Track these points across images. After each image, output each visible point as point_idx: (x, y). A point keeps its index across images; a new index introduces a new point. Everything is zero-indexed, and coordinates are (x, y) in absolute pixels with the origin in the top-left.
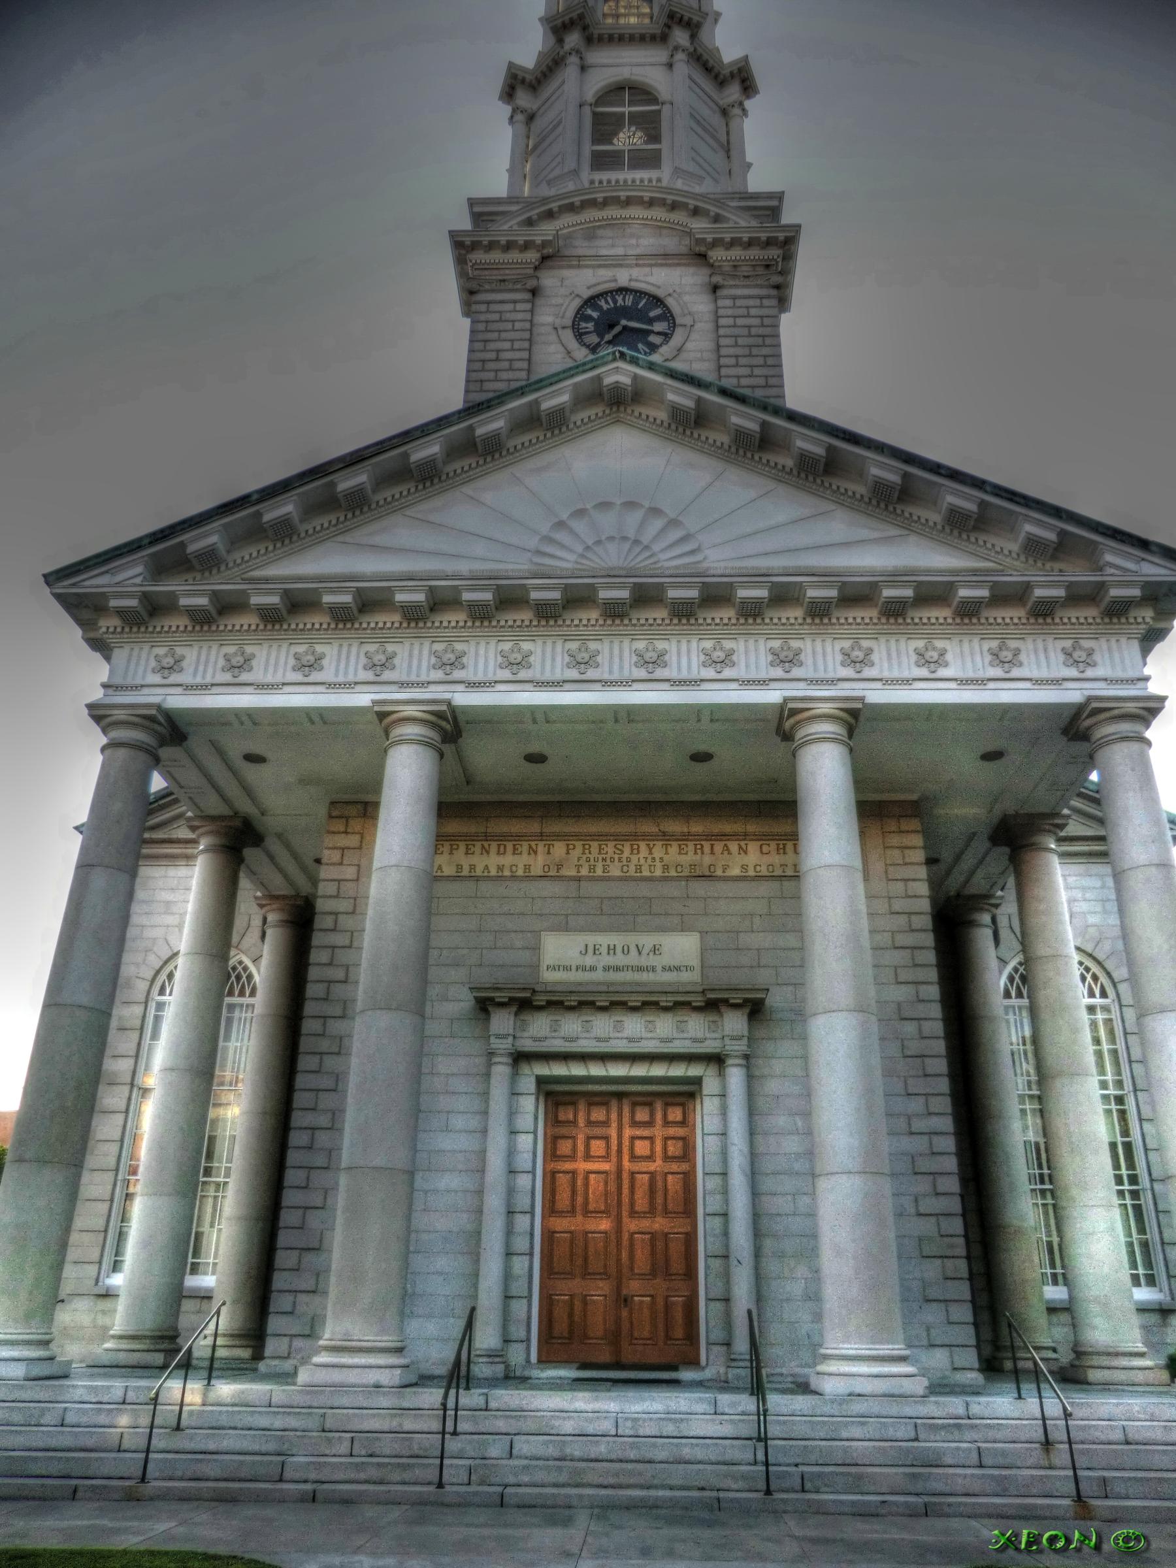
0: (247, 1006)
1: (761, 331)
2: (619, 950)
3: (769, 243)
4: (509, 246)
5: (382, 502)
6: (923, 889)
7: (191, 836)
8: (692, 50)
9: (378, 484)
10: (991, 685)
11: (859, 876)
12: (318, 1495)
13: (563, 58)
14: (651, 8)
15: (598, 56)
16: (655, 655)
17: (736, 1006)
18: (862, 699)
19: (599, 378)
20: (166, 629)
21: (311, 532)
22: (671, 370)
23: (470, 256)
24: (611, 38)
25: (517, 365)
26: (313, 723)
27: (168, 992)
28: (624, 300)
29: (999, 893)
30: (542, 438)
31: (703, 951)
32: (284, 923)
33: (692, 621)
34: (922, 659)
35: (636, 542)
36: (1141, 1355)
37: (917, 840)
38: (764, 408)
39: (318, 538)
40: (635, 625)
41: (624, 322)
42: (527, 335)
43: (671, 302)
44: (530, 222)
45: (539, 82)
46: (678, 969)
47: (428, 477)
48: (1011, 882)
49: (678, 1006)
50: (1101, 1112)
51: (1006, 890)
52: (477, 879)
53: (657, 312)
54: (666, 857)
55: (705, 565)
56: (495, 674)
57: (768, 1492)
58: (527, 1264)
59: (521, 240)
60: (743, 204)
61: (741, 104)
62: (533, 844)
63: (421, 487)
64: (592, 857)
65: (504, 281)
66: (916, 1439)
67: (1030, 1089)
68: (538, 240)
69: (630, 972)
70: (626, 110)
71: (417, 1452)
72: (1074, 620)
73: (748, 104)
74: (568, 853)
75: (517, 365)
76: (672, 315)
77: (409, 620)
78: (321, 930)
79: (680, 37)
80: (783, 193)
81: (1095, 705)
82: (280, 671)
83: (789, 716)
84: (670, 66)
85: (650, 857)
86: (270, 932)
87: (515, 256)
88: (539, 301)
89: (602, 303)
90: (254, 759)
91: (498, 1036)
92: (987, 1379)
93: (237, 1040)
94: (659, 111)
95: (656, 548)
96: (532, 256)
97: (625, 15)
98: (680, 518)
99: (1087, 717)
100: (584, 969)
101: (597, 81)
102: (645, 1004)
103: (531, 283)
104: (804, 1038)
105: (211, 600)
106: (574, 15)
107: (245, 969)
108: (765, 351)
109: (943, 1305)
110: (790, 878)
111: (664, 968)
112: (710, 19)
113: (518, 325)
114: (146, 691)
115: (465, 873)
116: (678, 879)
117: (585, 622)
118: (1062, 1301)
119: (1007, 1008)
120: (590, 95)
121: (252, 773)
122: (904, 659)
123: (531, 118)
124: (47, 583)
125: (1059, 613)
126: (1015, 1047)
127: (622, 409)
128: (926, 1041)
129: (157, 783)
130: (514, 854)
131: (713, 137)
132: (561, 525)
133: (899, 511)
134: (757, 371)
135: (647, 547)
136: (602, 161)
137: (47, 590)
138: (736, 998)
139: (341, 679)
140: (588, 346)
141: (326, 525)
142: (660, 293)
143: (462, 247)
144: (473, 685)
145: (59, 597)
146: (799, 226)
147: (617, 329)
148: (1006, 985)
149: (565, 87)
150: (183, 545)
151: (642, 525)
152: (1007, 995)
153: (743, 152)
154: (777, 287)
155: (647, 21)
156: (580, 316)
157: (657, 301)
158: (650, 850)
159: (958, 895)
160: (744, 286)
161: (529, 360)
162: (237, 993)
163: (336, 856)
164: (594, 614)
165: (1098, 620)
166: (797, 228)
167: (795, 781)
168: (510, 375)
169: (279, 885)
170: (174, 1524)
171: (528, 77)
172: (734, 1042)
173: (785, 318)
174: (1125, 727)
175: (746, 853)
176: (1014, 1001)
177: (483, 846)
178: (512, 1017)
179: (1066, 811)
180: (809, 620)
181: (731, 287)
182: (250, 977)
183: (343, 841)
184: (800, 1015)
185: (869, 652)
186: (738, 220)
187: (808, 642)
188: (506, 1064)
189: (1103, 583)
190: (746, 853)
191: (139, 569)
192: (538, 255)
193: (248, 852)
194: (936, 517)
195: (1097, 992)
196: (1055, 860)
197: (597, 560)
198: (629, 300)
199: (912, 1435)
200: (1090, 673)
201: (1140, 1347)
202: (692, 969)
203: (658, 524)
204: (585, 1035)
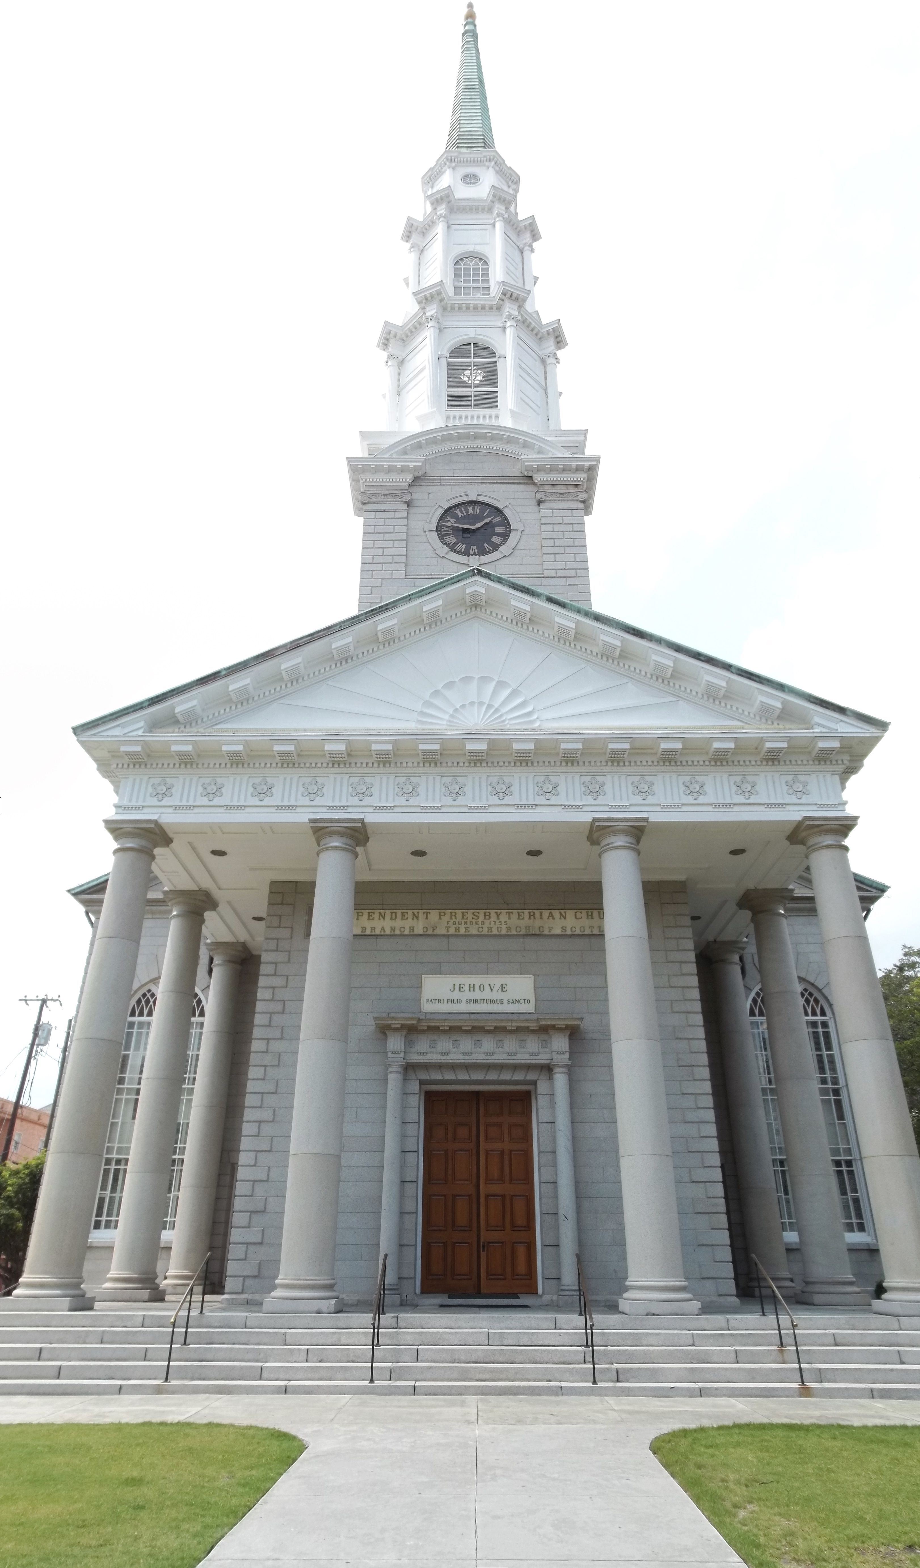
1: (572, 535)
2: (477, 988)
3: (578, 469)
10: (736, 808)
12: (288, 1389)
17: (560, 1030)
22: (513, 583)
26: (264, 832)
28: (473, 510)
29: (745, 939)
36: (851, 1283)
38: (579, 611)
43: (507, 512)
46: (519, 1002)
49: (519, 1030)
50: (819, 1104)
53: (498, 519)
54: (509, 921)
57: (782, 1345)
58: (414, 1220)
59: (399, 465)
61: (555, 354)
66: (693, 1345)
67: (770, 1084)
70: (472, 360)
71: (352, 1358)
74: (440, 918)
76: (508, 522)
79: (510, 308)
80: (587, 430)
81: (808, 823)
83: (597, 831)
85: (497, 921)
88: (412, 510)
89: (458, 512)
91: (394, 1052)
92: (741, 1301)
96: (408, 478)
100: (453, 1001)
102: (497, 1029)
103: (407, 498)
109: (824, 991)
115: (368, 932)
118: (796, 1243)
119: (752, 1023)
124: (75, 733)
127: (478, 609)
128: (694, 1055)
132: (436, 693)
137: (75, 738)
138: (561, 1024)
139: (286, 803)
140: (447, 545)
142: (500, 506)
145: (82, 743)
148: (751, 1007)
152: (752, 1013)
154: (583, 502)
158: (498, 916)
159: (715, 941)
162: (197, 1014)
166: (597, 459)
170: (200, 1409)
172: (559, 1056)
174: (829, 840)
175: (565, 918)
177: (380, 914)
184: (605, 1034)
185: (651, 785)
186: (555, 452)
187: (609, 777)
190: (565, 918)
191: (142, 724)
195: (818, 1012)
198: (477, 510)
199: (691, 1342)
200: (804, 800)
201: (850, 1277)
202: (529, 1001)
204: (454, 1050)
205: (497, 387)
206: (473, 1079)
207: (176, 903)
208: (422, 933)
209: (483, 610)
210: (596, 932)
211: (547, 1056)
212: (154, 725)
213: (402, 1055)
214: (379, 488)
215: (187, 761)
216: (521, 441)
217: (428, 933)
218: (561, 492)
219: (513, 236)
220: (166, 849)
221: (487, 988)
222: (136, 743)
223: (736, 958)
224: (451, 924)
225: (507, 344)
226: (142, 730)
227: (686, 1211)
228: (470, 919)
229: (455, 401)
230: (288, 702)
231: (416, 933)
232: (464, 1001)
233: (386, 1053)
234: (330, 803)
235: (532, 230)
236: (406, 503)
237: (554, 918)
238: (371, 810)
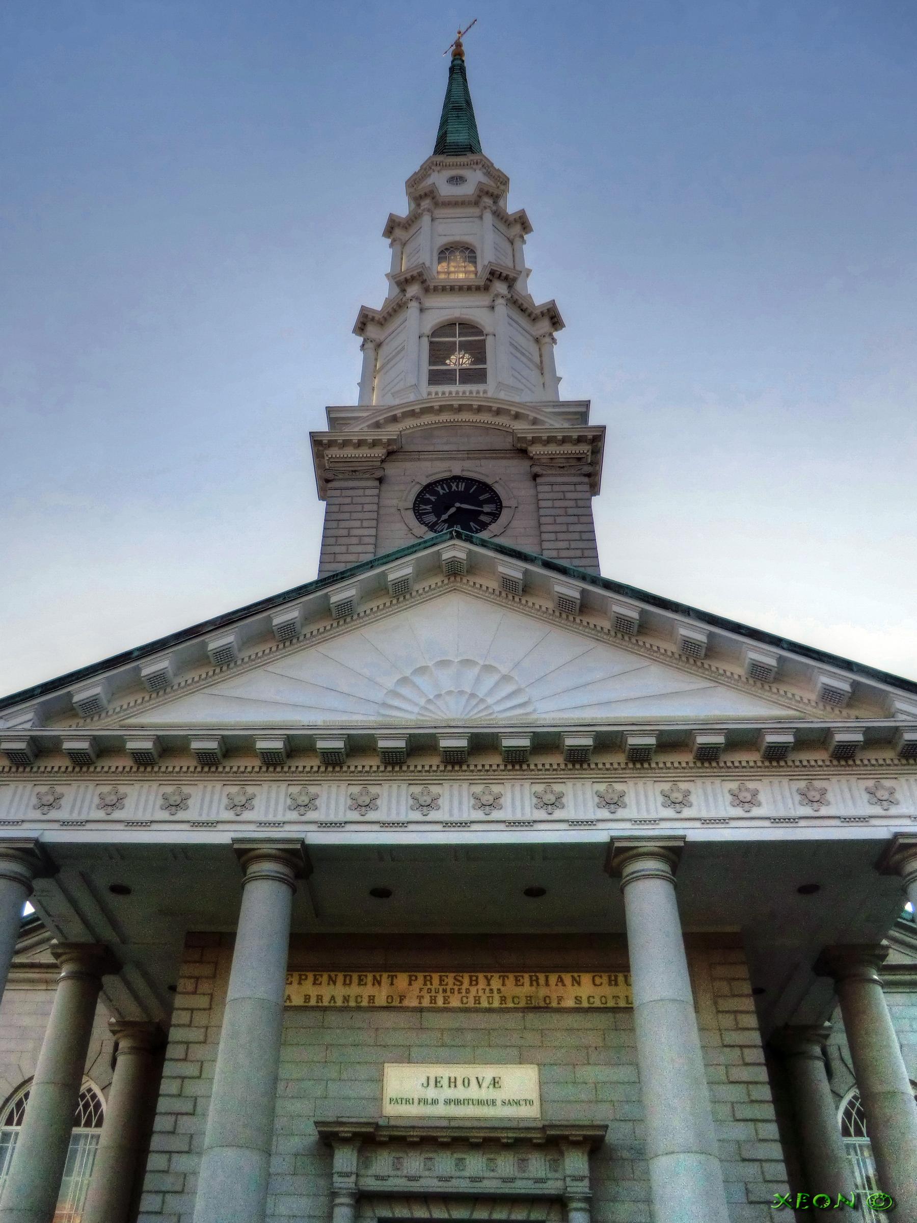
0: (93, 1136)
1: (576, 511)
2: (459, 1082)
3: (580, 440)
4: (360, 444)
5: (246, 659)
6: (752, 1021)
7: (52, 960)
8: (509, 296)
9: (244, 644)
10: (802, 823)
11: (691, 1009)
13: (405, 303)
14: (476, 267)
15: (432, 301)
16: (491, 798)
18: (683, 838)
19: (438, 553)
20: (49, 769)
21: (183, 684)
22: (501, 546)
23: (327, 452)
24: (444, 289)
25: (366, 540)
27: (16, 1119)
28: (457, 486)
29: (827, 1024)
30: (388, 604)
31: (541, 1084)
32: (134, 1050)
33: (525, 767)
34: (738, 800)
35: (473, 695)
37: (742, 971)
38: (584, 578)
39: (191, 688)
40: (472, 771)
41: (458, 505)
42: (375, 515)
43: (498, 488)
44: (377, 425)
45: (385, 319)
46: (518, 1103)
47: (288, 636)
48: (838, 1013)
51: (833, 1021)
52: (325, 1009)
53: (487, 496)
54: (503, 989)
55: (534, 716)
56: (345, 815)
59: (370, 439)
60: (557, 410)
61: (551, 334)
62: (378, 975)
63: (281, 646)
64: (433, 988)
65: (355, 471)
68: (385, 438)
69: (471, 1106)
70: (457, 339)
72: (873, 762)
73: (556, 334)
74: (410, 984)
75: (366, 540)
76: (499, 498)
77: (268, 765)
78: (172, 1060)
79: (500, 287)
82: (149, 810)
83: (616, 855)
84: (492, 308)
86: (121, 1060)
87: (364, 452)
88: (385, 487)
89: (439, 489)
90: (119, 890)
93: (79, 1175)
94: (484, 340)
95: (490, 701)
96: (380, 452)
97: (454, 272)
98: (512, 674)
99: (895, 854)
101: (433, 319)
103: (379, 474)
104: (646, 1177)
105: (91, 745)
106: (415, 273)
107: (94, 1097)
108: (579, 528)
110: (623, 1013)
111: (504, 1103)
112: (524, 274)
113: (367, 508)
114: (26, 826)
115: (313, 1002)
116: (516, 1010)
117: (427, 768)
119: (848, 1146)
120: (428, 328)
121: (116, 902)
122: (720, 799)
123: (379, 345)
125: (859, 755)
126: (861, 1191)
127: (458, 579)
129: (29, 909)
130: (359, 984)
131: (530, 360)
132: (404, 680)
133: (706, 666)
134: (574, 545)
135: (482, 700)
136: (436, 378)
140: (426, 525)
141: (196, 679)
142: (489, 481)
143: (318, 443)
144: (325, 825)
146: (604, 427)
147: (452, 510)
149: (406, 323)
150: (70, 695)
151: (478, 680)
152: (846, 1132)
153: (554, 370)
154: (589, 475)
155: (472, 276)
156: (420, 500)
157: (485, 487)
160: (560, 475)
161: (376, 536)
163: (189, 985)
164: (435, 761)
165: (896, 762)
167: (625, 923)
168: (360, 549)
169: (134, 1012)
171: (377, 317)
173: (595, 500)
175: (579, 984)
176: (854, 1140)
178: (355, 1154)
179: (885, 942)
180: (631, 765)
181: (548, 475)
182: (98, 1105)
183: (197, 970)
184: (640, 1154)
188: (348, 1205)
189: (897, 728)
190: (579, 984)
192: (384, 451)
193: (109, 981)
194: (739, 671)
196: (879, 990)
197: (440, 713)
200: (893, 811)
202: (531, 1102)
203: (490, 681)
204: (427, 1173)
205: (485, 363)
206: (454, 1217)
207: (66, 961)
208: (385, 1004)
209: (465, 581)
210: (622, 1004)
211: (559, 1184)
212: (46, 716)
213: (353, 1178)
214: (346, 464)
215: (82, 762)
216: (513, 413)
217: (394, 1004)
218: (562, 465)
219: (502, 227)
220: (51, 880)
221: (474, 1082)
222: (18, 738)
223: (817, 1050)
224: (424, 993)
225: (494, 319)
226: (30, 724)
227: (486, 1119)
228: (450, 986)
229: (436, 378)
230: (216, 692)
231: (377, 1004)
232: (441, 1102)
233: (331, 1175)
234: (263, 818)
235: (522, 223)
236: (377, 479)
237: (564, 985)
238: (313, 827)
